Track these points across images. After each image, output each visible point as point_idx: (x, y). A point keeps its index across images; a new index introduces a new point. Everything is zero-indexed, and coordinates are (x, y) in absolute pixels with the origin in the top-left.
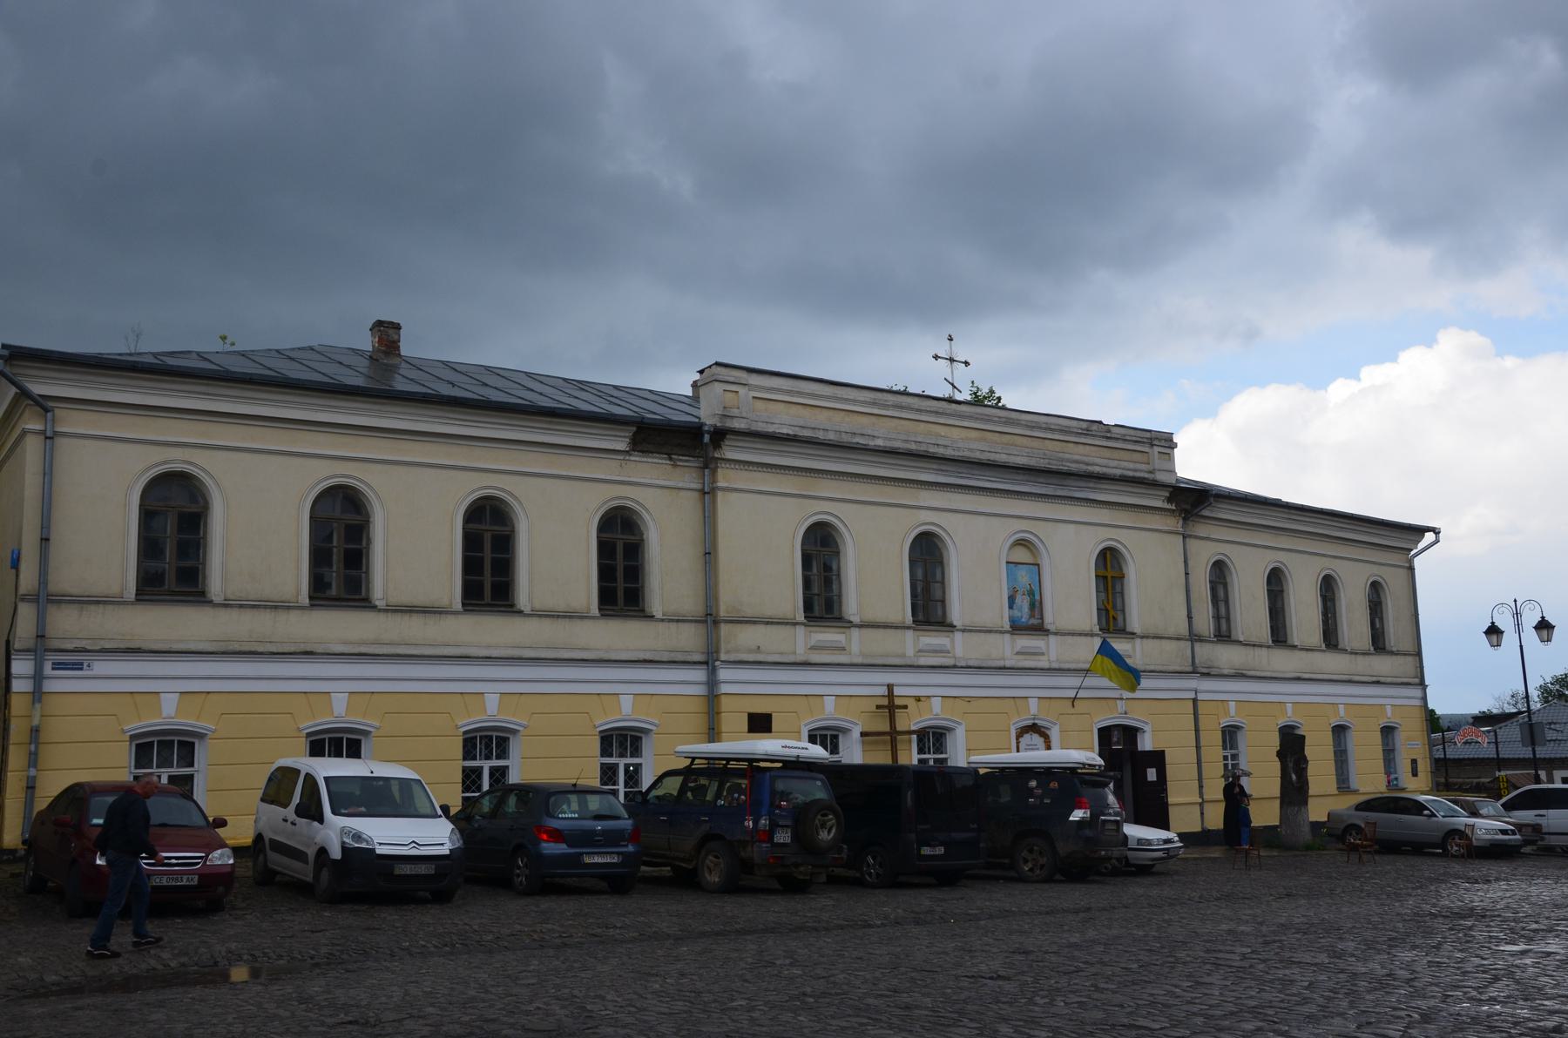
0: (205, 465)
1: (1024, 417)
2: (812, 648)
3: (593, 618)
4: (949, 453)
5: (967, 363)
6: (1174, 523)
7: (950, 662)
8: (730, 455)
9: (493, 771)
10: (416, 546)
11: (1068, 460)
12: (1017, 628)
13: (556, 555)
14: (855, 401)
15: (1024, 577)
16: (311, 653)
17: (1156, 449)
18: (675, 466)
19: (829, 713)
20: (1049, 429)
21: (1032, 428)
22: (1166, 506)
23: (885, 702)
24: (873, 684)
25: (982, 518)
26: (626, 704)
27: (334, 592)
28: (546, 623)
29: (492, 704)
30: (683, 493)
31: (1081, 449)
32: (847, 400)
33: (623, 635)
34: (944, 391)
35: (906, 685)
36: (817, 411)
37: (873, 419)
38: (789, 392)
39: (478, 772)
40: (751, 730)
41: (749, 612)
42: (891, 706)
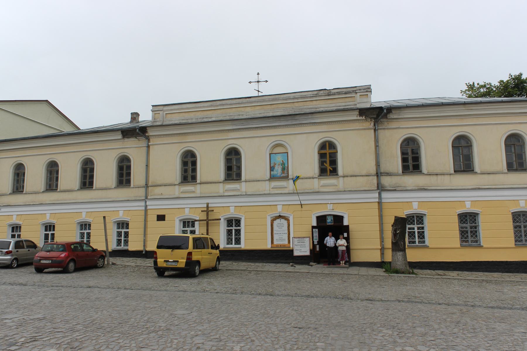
0: (23, 161)
1: (282, 96)
2: (273, 188)
3: (505, 173)
4: (245, 117)
5: (258, 74)
6: (370, 124)
7: (239, 193)
8: (151, 134)
9: (87, 233)
10: (70, 175)
11: (306, 109)
12: (272, 178)
13: (105, 172)
14: (204, 107)
15: (279, 159)
16: (10, 205)
17: (359, 94)
18: (139, 140)
19: (188, 214)
20: (339, 93)
21: (286, 99)
22: (359, 118)
23: (205, 209)
24: (202, 204)
25: (258, 139)
26: (415, 205)
27: (87, 186)
28: (100, 191)
29: (468, 205)
30: (142, 148)
31: (315, 102)
32: (200, 107)
33: (124, 193)
34: (256, 94)
35: (214, 203)
36: (190, 113)
37: (213, 111)
38: (221, 105)
39: (121, 232)
40: (158, 220)
41: (159, 183)
42: (208, 210)
